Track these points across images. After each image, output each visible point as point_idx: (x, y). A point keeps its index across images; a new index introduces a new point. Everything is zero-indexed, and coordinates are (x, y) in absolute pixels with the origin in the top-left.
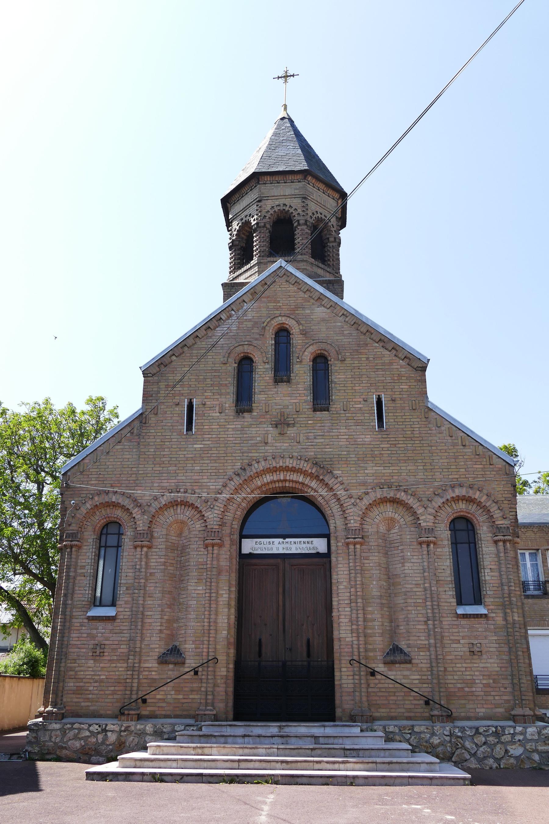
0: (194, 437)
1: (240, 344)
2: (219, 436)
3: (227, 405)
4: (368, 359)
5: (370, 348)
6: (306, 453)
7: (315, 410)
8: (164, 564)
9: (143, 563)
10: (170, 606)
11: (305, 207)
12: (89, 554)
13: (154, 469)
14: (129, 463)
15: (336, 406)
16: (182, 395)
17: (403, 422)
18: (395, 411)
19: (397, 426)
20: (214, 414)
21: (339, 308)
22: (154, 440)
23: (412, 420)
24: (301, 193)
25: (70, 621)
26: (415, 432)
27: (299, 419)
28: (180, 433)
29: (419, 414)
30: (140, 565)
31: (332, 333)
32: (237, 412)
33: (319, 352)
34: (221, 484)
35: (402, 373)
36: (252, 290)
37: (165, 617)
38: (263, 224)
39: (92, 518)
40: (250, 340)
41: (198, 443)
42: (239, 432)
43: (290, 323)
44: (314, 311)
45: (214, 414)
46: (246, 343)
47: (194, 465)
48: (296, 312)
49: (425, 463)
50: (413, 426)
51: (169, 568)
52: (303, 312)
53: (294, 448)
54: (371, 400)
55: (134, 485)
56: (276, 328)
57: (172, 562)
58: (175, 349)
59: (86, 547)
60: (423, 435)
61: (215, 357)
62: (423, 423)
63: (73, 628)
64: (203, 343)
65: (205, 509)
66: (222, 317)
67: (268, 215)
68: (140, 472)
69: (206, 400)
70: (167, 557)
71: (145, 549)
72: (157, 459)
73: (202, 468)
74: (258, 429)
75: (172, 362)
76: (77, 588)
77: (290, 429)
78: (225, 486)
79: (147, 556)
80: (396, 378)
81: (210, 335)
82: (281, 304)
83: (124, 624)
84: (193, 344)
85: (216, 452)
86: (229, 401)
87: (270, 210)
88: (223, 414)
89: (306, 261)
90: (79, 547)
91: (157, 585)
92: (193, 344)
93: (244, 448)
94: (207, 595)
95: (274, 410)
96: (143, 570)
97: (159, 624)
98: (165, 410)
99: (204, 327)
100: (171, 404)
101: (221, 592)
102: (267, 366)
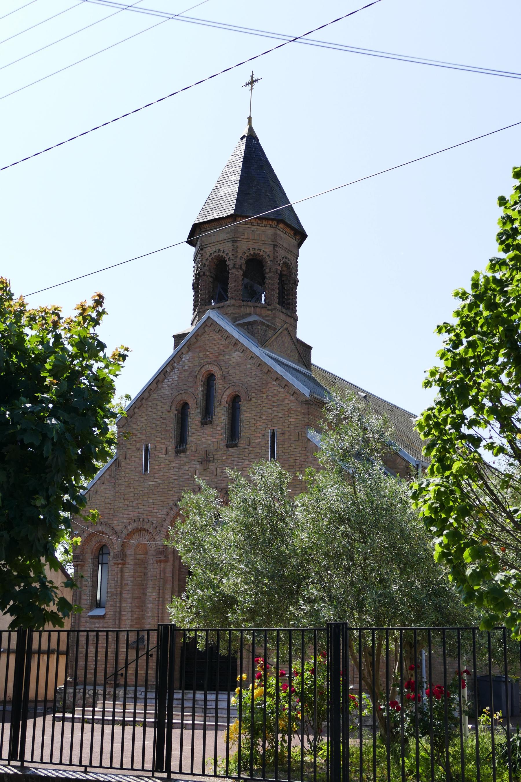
0: (148, 476)
1: (179, 393)
2: (165, 474)
3: (170, 448)
4: (267, 396)
5: (270, 386)
6: (221, 485)
7: (228, 447)
8: (133, 576)
9: (119, 577)
10: (139, 608)
11: (235, 250)
12: (89, 570)
13: (125, 503)
14: (109, 500)
15: (243, 442)
16: (141, 441)
17: (288, 452)
18: (283, 443)
19: (284, 457)
20: (162, 456)
21: (249, 351)
22: (124, 480)
23: (295, 450)
24: (231, 237)
25: (79, 619)
26: (297, 461)
27: (217, 456)
28: (140, 474)
29: (301, 444)
30: (117, 578)
31: (243, 375)
32: (176, 453)
33: (234, 393)
34: (165, 513)
35: (292, 407)
36: (188, 343)
37: (135, 616)
38: (202, 273)
39: (90, 543)
40: (186, 388)
41: (151, 480)
42: (177, 470)
43: (215, 370)
44: (233, 356)
45: (162, 456)
46: (183, 392)
47: (149, 499)
48: (219, 358)
49: (302, 487)
50: (295, 456)
51: (137, 579)
52: (224, 358)
53: (213, 480)
54: (279, 430)
55: (112, 517)
56: (205, 375)
57: (140, 574)
58: (136, 403)
59: (87, 565)
60: (302, 463)
61: (163, 406)
62: (303, 452)
63: (82, 624)
64: (156, 395)
65: (155, 533)
66: (168, 370)
67: (207, 263)
68: (116, 507)
69: (156, 444)
70: (135, 571)
71: (120, 566)
72: (126, 496)
73: (154, 501)
74: (189, 466)
75: (135, 413)
76: (83, 596)
77: (210, 464)
78: (168, 514)
79: (122, 569)
80: (286, 413)
81: (160, 387)
82: (208, 353)
83: (110, 621)
84: (149, 397)
85: (162, 487)
86: (171, 444)
87: (209, 258)
88: (167, 456)
89: (233, 306)
90: (83, 566)
91: (129, 592)
92: (149, 397)
93: (180, 483)
94: (157, 599)
95: (200, 449)
96: (119, 582)
97: (130, 621)
98: (131, 455)
99: (155, 381)
100: (134, 449)
101: (167, 597)
102: (197, 411)
